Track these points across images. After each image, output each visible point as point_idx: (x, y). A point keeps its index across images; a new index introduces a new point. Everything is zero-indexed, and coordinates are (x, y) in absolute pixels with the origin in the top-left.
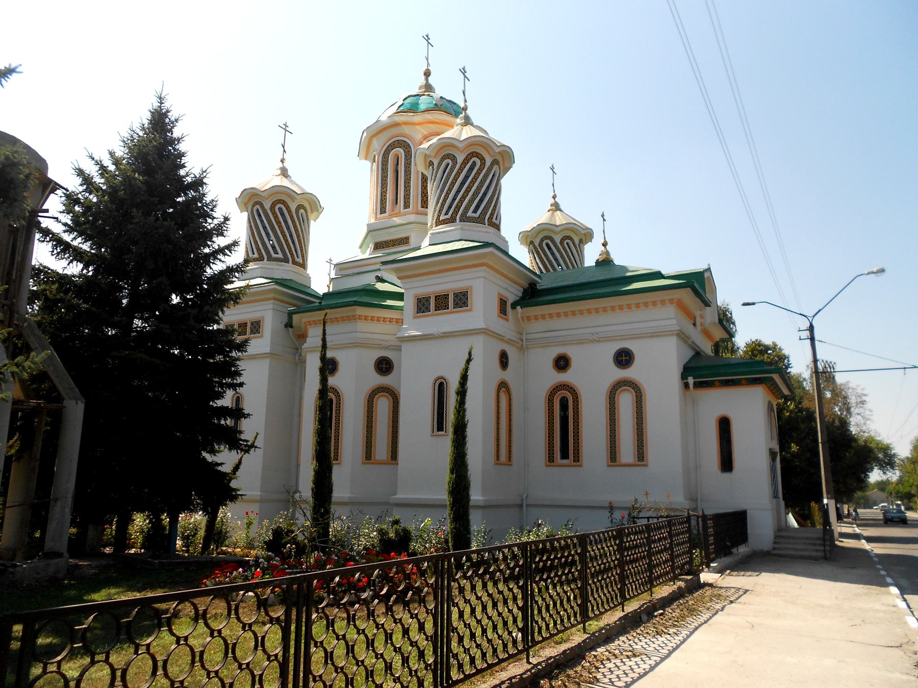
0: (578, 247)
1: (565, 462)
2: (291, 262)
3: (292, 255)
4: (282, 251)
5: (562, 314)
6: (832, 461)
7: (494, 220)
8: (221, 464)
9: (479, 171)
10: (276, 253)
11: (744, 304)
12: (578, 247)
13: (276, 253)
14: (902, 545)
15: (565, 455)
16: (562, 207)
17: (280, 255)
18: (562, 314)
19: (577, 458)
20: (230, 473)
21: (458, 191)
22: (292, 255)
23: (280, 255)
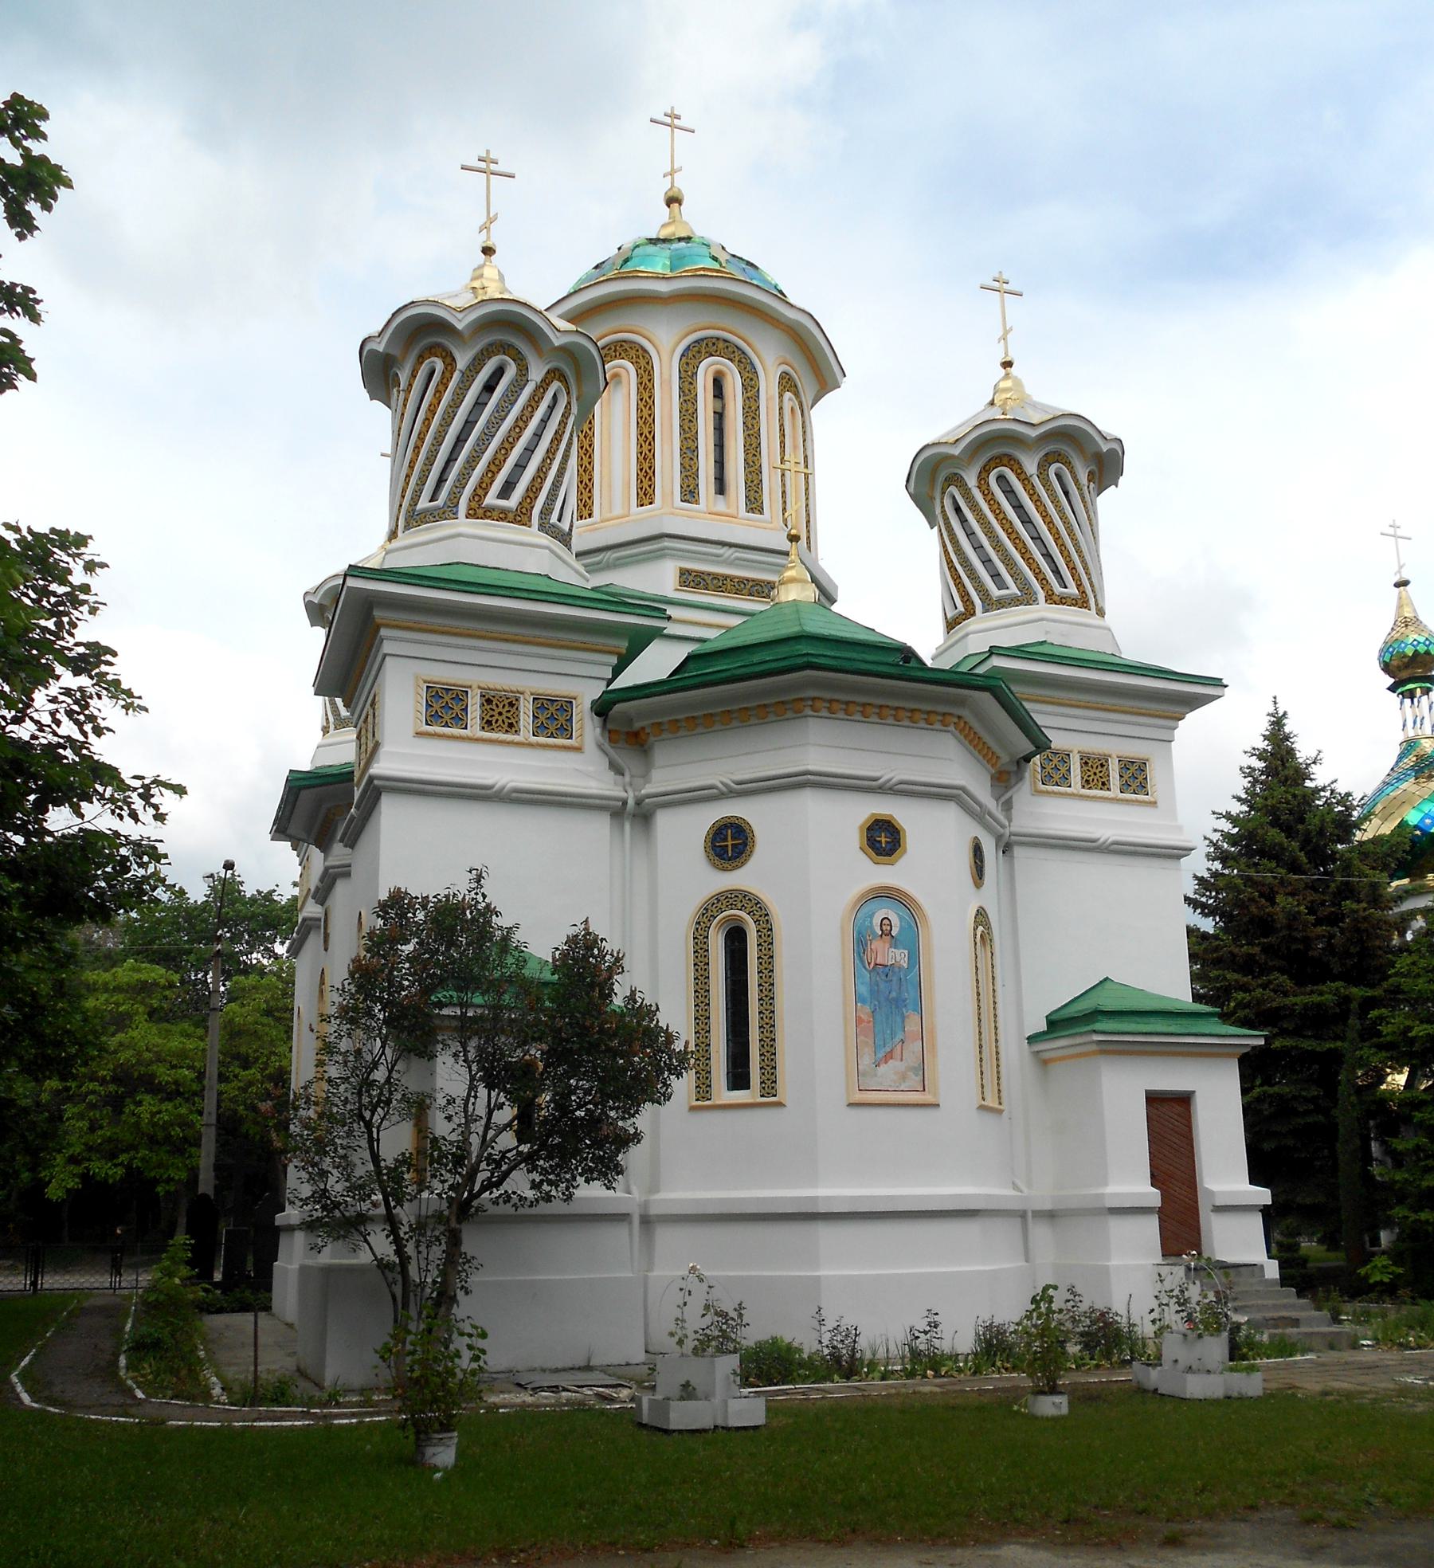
0: (1036, 481)
1: (740, 1096)
2: (1041, 595)
3: (1043, 581)
4: (1015, 580)
5: (526, 710)
6: (733, 974)
7: (554, 519)
8: (458, 1306)
9: (521, 424)
10: (1002, 585)
11: (1382, 534)
12: (1036, 481)
13: (1002, 585)
14: (925, 1194)
15: (739, 1078)
16: (991, 398)
17: (1073, 590)
18: (526, 710)
19: (770, 1086)
20: (208, 1308)
21: (520, 467)
22: (1043, 581)
23: (1073, 590)
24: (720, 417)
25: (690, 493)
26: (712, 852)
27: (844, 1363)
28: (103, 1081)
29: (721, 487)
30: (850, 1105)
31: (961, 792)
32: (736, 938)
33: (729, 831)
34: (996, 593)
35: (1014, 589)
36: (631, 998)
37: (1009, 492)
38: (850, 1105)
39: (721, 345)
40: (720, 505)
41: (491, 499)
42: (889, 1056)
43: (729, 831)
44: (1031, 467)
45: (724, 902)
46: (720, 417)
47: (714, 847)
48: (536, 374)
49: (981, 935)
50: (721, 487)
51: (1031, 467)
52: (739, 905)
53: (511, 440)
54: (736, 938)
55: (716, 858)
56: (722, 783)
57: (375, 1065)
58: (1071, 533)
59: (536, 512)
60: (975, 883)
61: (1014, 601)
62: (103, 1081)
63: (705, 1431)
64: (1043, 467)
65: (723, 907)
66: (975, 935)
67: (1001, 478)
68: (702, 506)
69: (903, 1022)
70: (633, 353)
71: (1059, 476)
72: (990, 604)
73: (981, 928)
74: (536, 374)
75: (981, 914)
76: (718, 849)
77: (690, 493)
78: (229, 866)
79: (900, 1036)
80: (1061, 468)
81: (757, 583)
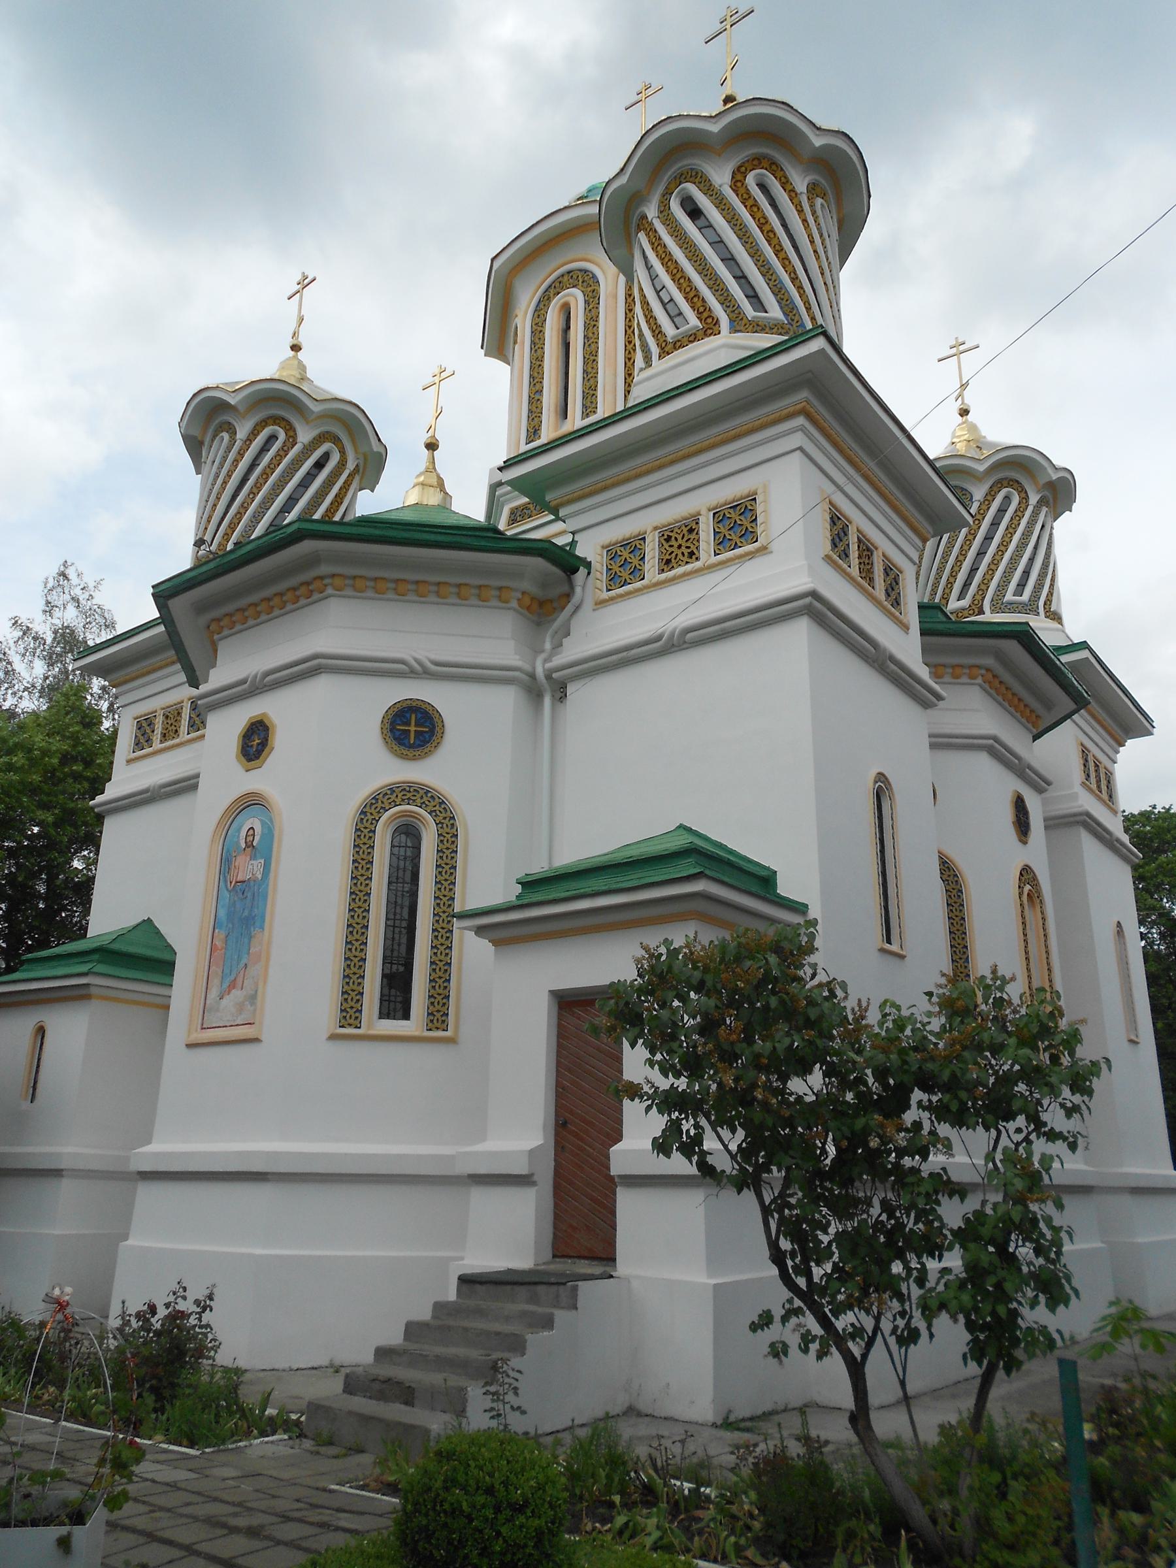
26: (389, 734)
30: (189, 1046)
31: (991, 742)
32: (408, 833)
33: (413, 716)
38: (189, 1046)
41: (1009, 596)
42: (232, 986)
43: (413, 716)
44: (721, 177)
45: (400, 795)
47: (392, 730)
48: (1034, 499)
49: (1028, 895)
51: (721, 177)
52: (419, 801)
53: (1005, 543)
54: (408, 833)
55: (394, 742)
56: (416, 660)
59: (1041, 603)
60: (1021, 841)
63: (321, 1367)
64: (737, 183)
65: (398, 801)
66: (1020, 895)
69: (249, 943)
71: (762, 187)
73: (1027, 888)
74: (1034, 499)
75: (1027, 875)
76: (398, 733)
79: (244, 961)
80: (763, 175)
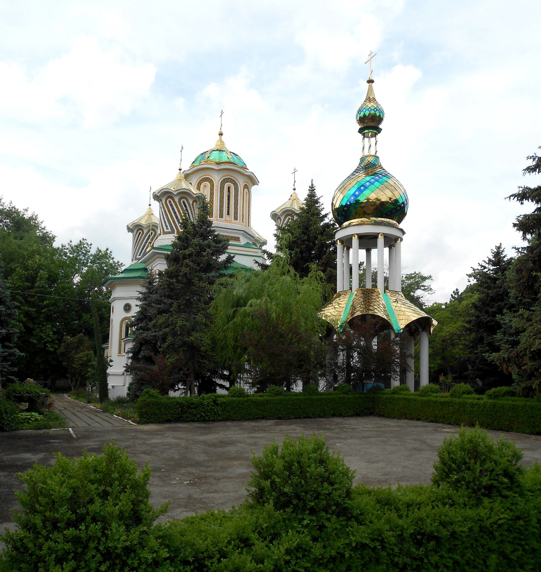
24: (229, 197)
25: (221, 216)
27: (398, 370)
28: (507, 369)
29: (228, 214)
34: (166, 230)
35: (170, 230)
36: (528, 200)
37: (171, 205)
39: (229, 180)
40: (228, 219)
46: (229, 197)
50: (228, 214)
51: (177, 200)
57: (342, 525)
58: (165, 212)
61: (169, 233)
62: (507, 369)
67: (170, 201)
68: (224, 219)
70: (209, 181)
72: (165, 233)
77: (221, 216)
78: (522, 203)
81: (235, 237)
